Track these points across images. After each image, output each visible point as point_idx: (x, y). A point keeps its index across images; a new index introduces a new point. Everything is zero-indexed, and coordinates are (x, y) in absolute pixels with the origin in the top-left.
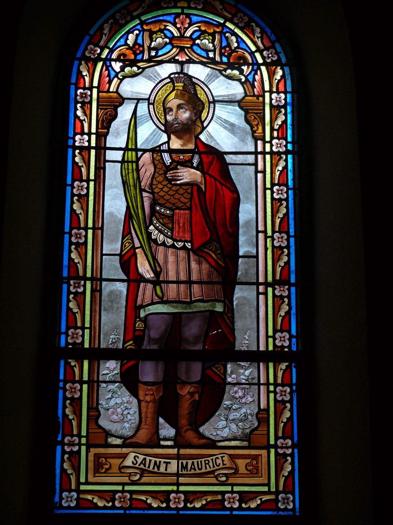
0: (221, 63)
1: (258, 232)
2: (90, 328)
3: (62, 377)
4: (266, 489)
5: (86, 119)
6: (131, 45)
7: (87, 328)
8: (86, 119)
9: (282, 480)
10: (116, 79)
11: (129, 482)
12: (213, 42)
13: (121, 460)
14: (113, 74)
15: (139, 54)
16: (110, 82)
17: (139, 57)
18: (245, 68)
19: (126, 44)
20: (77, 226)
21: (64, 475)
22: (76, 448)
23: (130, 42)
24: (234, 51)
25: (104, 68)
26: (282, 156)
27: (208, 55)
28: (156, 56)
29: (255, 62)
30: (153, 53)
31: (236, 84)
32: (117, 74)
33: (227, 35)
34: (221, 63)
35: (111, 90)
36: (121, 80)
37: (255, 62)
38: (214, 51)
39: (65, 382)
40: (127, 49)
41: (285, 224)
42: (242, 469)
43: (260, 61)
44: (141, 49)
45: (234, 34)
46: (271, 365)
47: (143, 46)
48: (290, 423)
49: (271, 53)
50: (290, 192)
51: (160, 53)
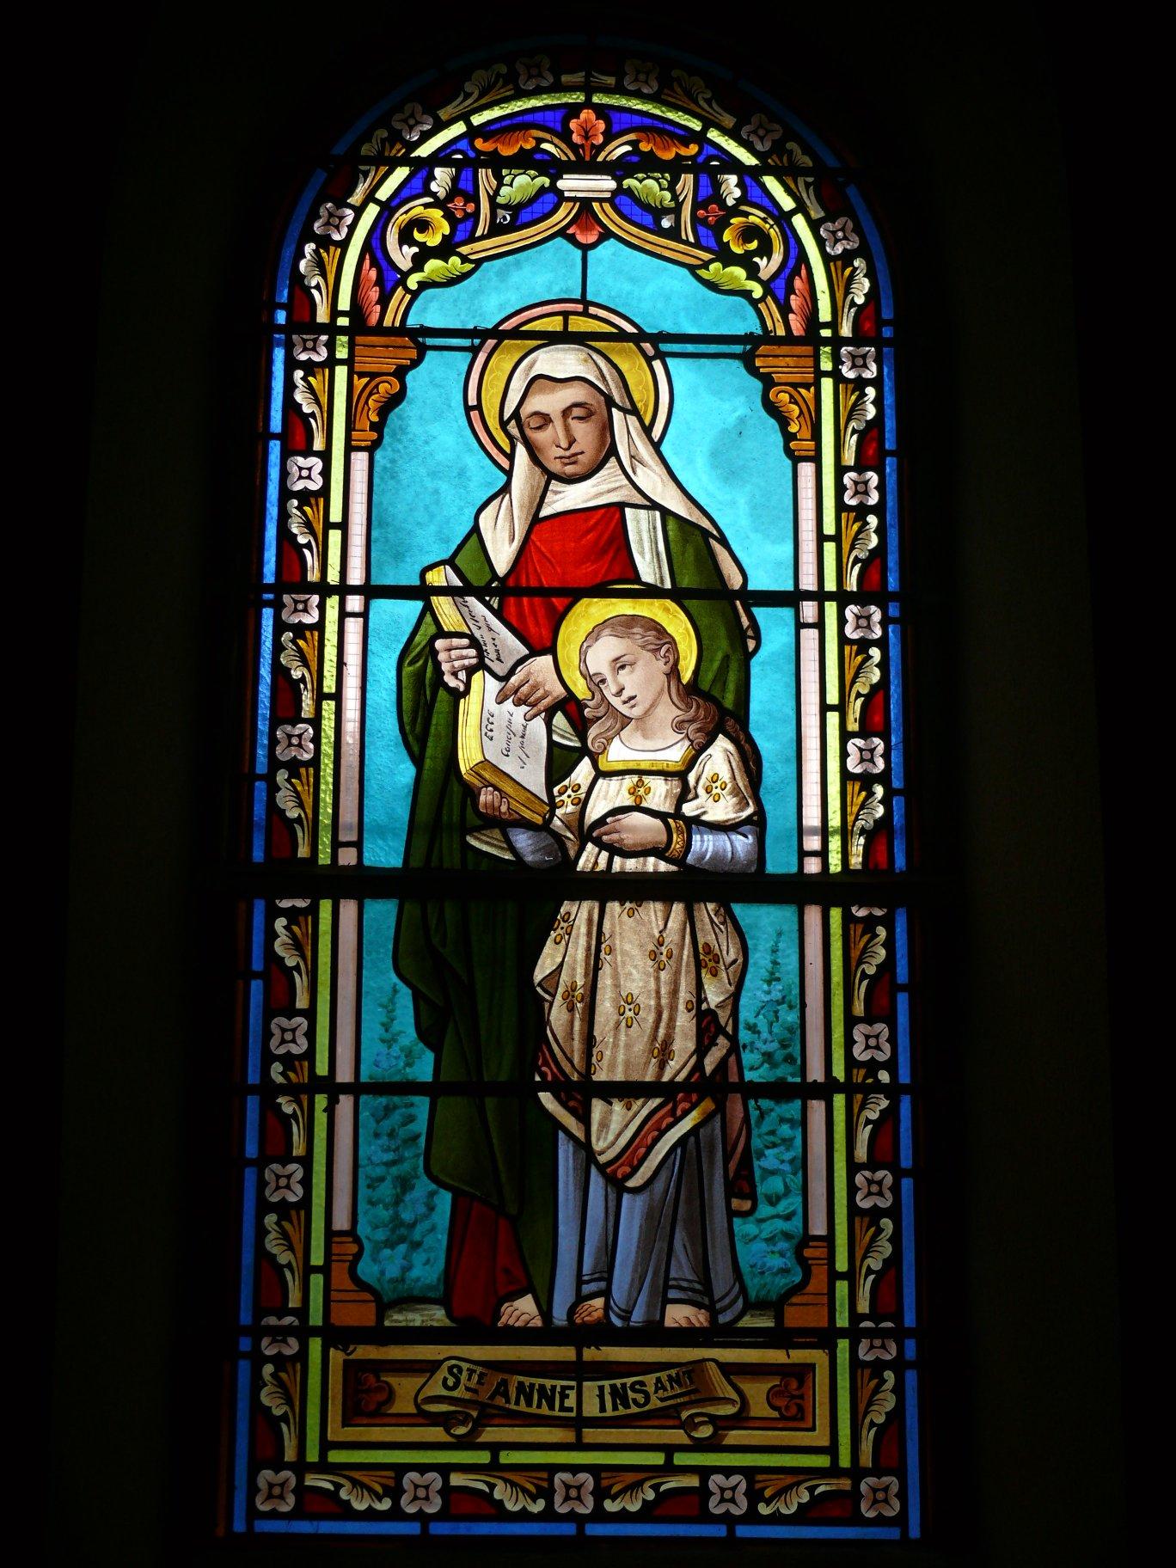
3: (269, 576)
4: (823, 1461)
5: (307, 675)
6: (442, 194)
8: (307, 675)
9: (864, 1134)
10: (400, 291)
11: (449, 1439)
13: (422, 1380)
16: (384, 301)
22: (292, 1347)
25: (367, 262)
30: (505, 216)
35: (387, 322)
36: (415, 295)
38: (676, 211)
39: (262, 1162)
40: (426, 206)
42: (760, 1408)
44: (470, 208)
46: (836, 914)
48: (875, 433)
49: (842, 229)
50: (907, 1184)
51: (525, 216)
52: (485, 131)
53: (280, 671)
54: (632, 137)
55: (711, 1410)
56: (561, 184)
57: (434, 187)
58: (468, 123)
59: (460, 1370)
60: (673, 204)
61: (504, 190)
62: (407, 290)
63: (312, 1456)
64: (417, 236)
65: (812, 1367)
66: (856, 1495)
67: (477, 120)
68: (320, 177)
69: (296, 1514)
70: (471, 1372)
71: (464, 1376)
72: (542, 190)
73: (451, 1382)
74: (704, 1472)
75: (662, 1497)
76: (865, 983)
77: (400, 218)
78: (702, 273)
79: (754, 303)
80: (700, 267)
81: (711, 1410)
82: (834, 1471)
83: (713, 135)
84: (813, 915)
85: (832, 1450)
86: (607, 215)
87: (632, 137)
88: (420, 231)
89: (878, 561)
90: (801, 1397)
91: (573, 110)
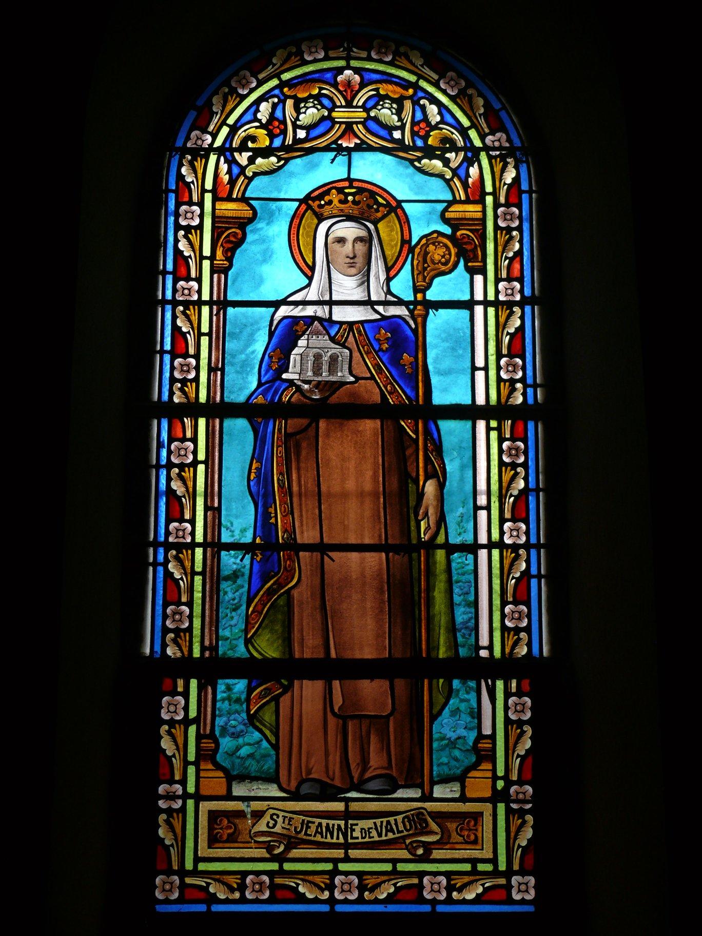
0: (415, 148)
1: (474, 369)
2: (205, 462)
4: (489, 867)
5: (177, 755)
6: (264, 121)
7: (201, 462)
8: (177, 755)
9: (506, 339)
10: (242, 178)
12: (399, 113)
14: (236, 170)
15: (278, 136)
17: (277, 143)
18: (451, 155)
19: (256, 119)
20: (168, 777)
21: (169, 581)
23: (263, 115)
24: (436, 127)
26: (514, 309)
27: (391, 135)
28: (306, 140)
29: (468, 145)
30: (301, 134)
31: (437, 183)
32: (243, 169)
33: (422, 102)
34: (415, 148)
36: (250, 179)
37: (468, 145)
38: (402, 128)
40: (257, 127)
41: (517, 341)
43: (478, 143)
45: (434, 100)
47: (284, 122)
52: (289, 83)
53: (176, 329)
54: (373, 87)
55: (423, 839)
56: (334, 114)
57: (259, 116)
58: (280, 79)
59: (278, 816)
60: (399, 124)
61: (301, 117)
62: (246, 177)
63: (189, 865)
64: (250, 145)
65: (481, 814)
66: (509, 887)
67: (286, 76)
68: (192, 115)
69: (180, 901)
70: (285, 817)
71: (280, 820)
72: (323, 119)
73: (271, 825)
74: (421, 875)
75: (398, 889)
76: (512, 499)
77: (241, 133)
78: (416, 164)
79: (448, 182)
80: (415, 160)
81: (423, 839)
82: (495, 873)
83: (423, 84)
84: (481, 425)
85: (494, 861)
86: (360, 129)
87: (373, 87)
88: (253, 142)
89: (518, 259)
90: (476, 830)
91: (340, 71)
